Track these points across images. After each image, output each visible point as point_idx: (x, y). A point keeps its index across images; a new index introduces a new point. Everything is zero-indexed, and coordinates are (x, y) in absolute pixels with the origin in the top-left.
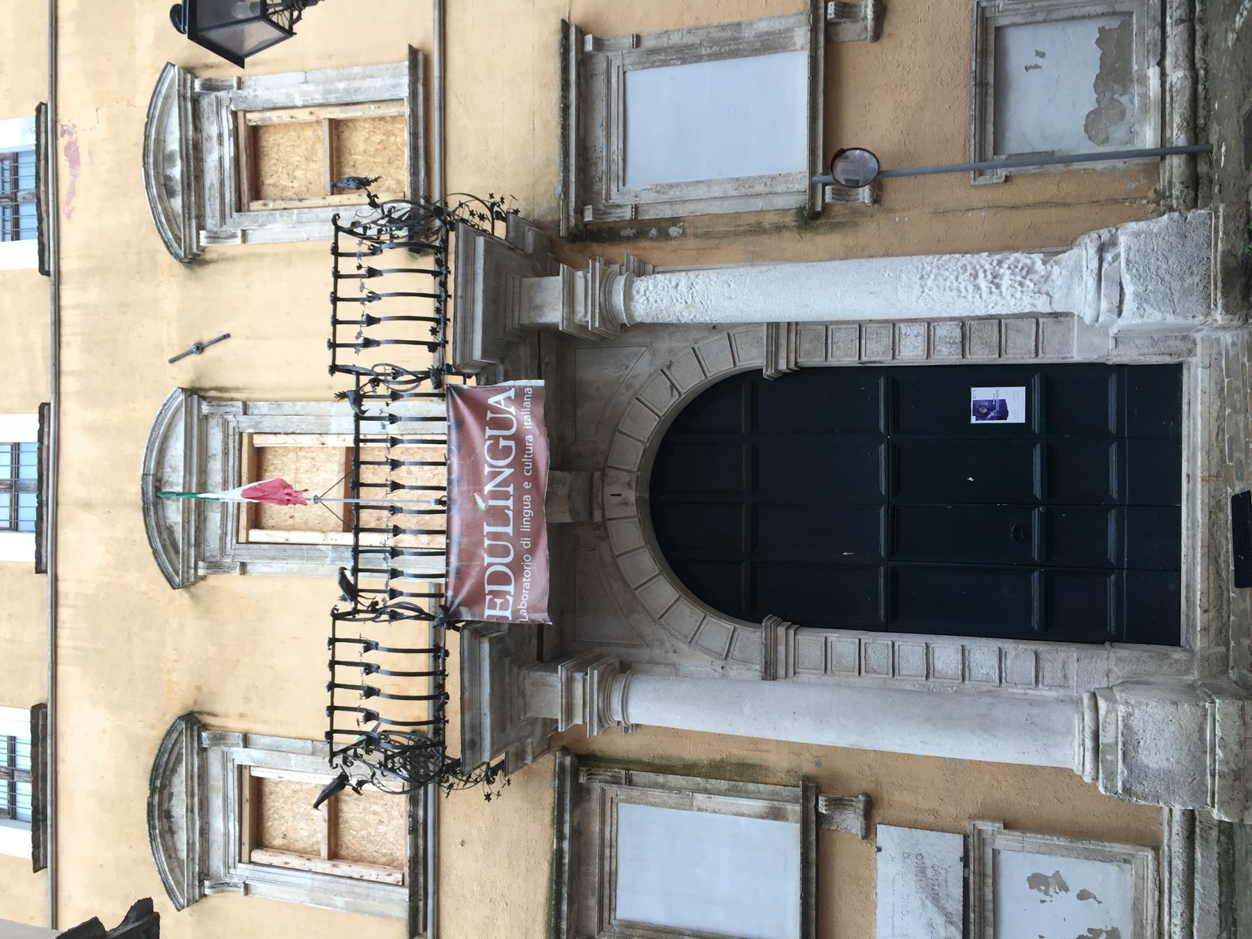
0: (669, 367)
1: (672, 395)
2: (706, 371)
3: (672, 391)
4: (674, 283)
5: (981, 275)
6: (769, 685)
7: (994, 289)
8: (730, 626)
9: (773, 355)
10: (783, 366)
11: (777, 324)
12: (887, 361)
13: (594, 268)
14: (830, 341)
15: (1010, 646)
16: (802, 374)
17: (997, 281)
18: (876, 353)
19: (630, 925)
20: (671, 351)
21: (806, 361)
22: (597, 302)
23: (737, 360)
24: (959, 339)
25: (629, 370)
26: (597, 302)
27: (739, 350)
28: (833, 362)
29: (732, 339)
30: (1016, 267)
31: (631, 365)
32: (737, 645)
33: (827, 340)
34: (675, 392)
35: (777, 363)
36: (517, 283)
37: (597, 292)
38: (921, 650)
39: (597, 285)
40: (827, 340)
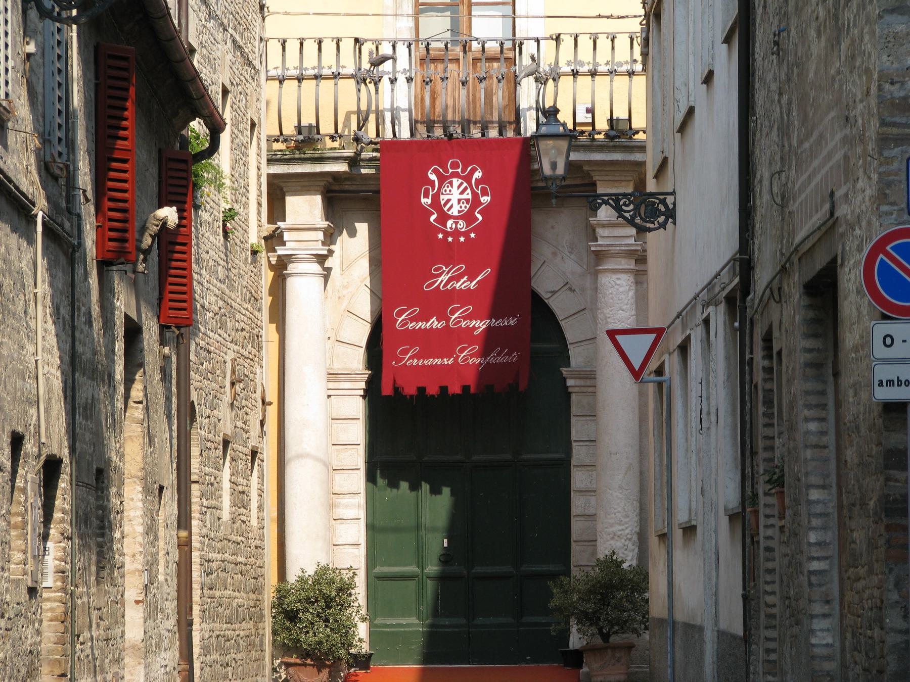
0: (570, 289)
1: (547, 292)
2: (566, 321)
3: (551, 292)
4: (624, 307)
5: (620, 528)
6: (324, 376)
7: (611, 536)
8: (574, 444)
9: (579, 375)
10: (569, 382)
11: (595, 378)
12: (574, 462)
13: (637, 245)
14: (588, 418)
15: (362, 551)
16: (566, 395)
17: (616, 537)
18: (579, 453)
19: (453, 395)
20: (583, 290)
21: (574, 398)
22: (610, 248)
23: (575, 345)
24: (587, 512)
25: (568, 254)
26: (610, 248)
27: (583, 347)
28: (573, 420)
29: (591, 342)
30: (626, 550)
31: (572, 256)
32: (349, 349)
33: (590, 416)
34: (550, 295)
35: (572, 378)
36: (629, 178)
37: (618, 248)
38: (354, 489)
39: (623, 248)
40: (590, 416)
